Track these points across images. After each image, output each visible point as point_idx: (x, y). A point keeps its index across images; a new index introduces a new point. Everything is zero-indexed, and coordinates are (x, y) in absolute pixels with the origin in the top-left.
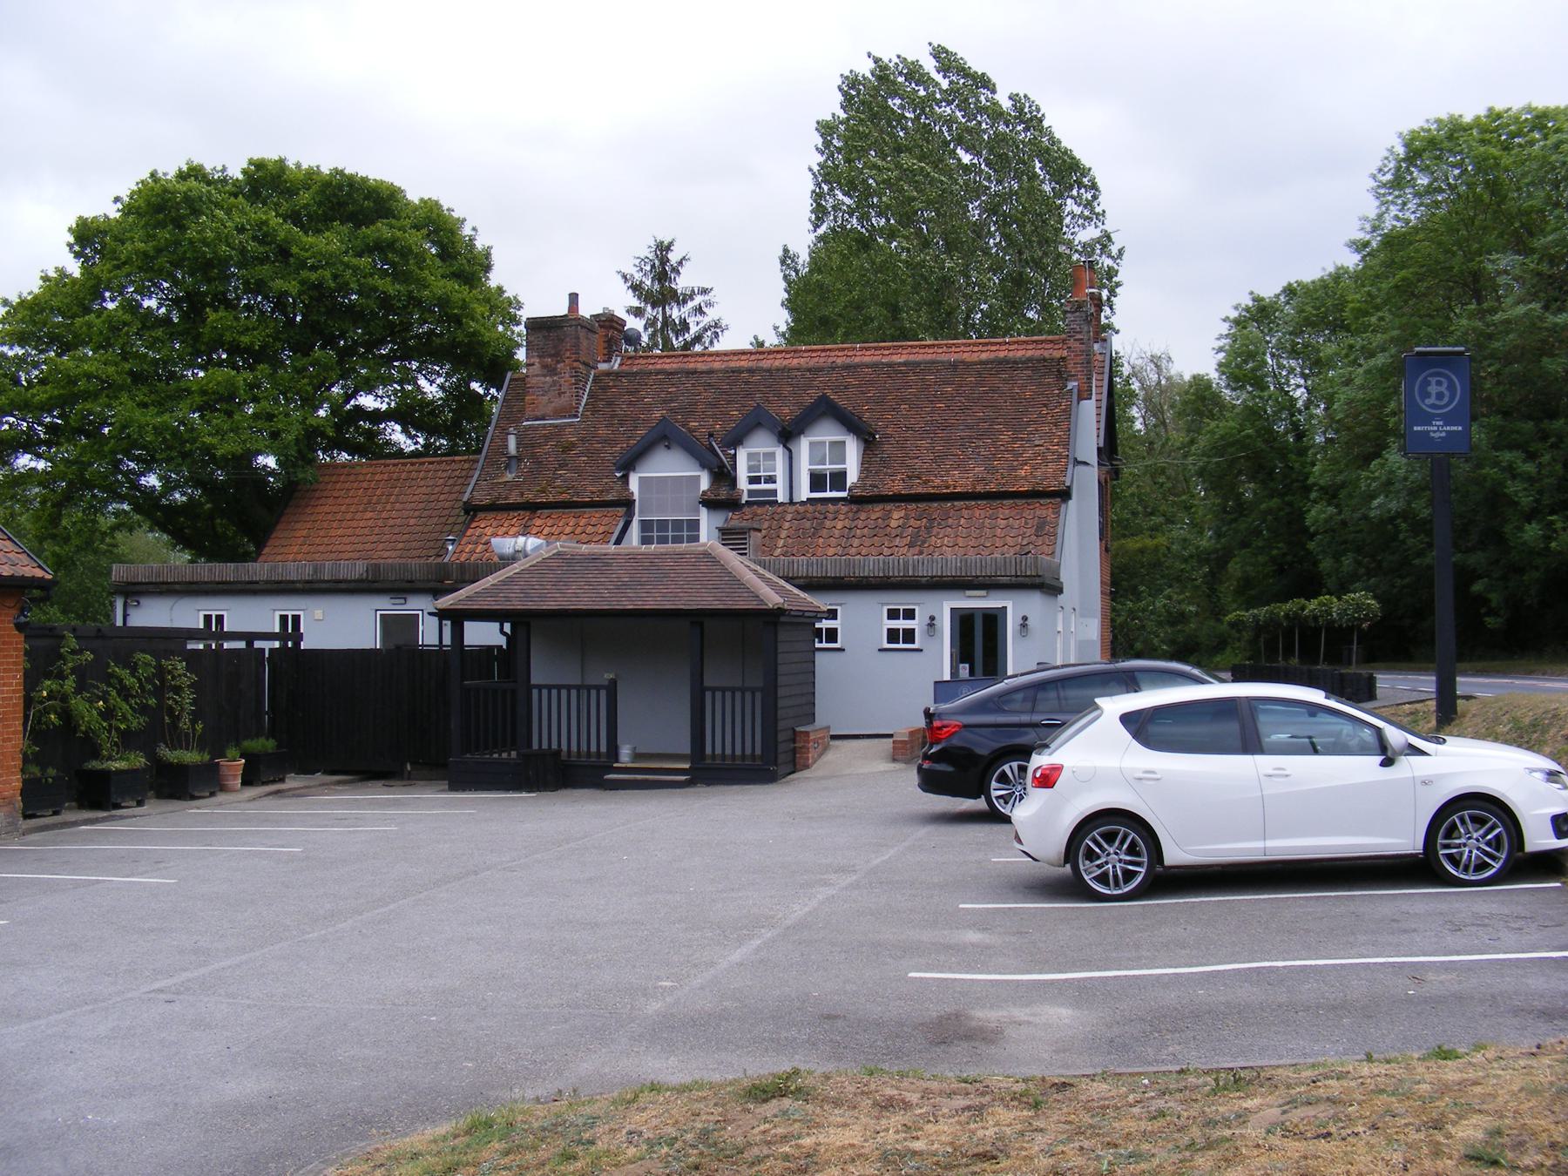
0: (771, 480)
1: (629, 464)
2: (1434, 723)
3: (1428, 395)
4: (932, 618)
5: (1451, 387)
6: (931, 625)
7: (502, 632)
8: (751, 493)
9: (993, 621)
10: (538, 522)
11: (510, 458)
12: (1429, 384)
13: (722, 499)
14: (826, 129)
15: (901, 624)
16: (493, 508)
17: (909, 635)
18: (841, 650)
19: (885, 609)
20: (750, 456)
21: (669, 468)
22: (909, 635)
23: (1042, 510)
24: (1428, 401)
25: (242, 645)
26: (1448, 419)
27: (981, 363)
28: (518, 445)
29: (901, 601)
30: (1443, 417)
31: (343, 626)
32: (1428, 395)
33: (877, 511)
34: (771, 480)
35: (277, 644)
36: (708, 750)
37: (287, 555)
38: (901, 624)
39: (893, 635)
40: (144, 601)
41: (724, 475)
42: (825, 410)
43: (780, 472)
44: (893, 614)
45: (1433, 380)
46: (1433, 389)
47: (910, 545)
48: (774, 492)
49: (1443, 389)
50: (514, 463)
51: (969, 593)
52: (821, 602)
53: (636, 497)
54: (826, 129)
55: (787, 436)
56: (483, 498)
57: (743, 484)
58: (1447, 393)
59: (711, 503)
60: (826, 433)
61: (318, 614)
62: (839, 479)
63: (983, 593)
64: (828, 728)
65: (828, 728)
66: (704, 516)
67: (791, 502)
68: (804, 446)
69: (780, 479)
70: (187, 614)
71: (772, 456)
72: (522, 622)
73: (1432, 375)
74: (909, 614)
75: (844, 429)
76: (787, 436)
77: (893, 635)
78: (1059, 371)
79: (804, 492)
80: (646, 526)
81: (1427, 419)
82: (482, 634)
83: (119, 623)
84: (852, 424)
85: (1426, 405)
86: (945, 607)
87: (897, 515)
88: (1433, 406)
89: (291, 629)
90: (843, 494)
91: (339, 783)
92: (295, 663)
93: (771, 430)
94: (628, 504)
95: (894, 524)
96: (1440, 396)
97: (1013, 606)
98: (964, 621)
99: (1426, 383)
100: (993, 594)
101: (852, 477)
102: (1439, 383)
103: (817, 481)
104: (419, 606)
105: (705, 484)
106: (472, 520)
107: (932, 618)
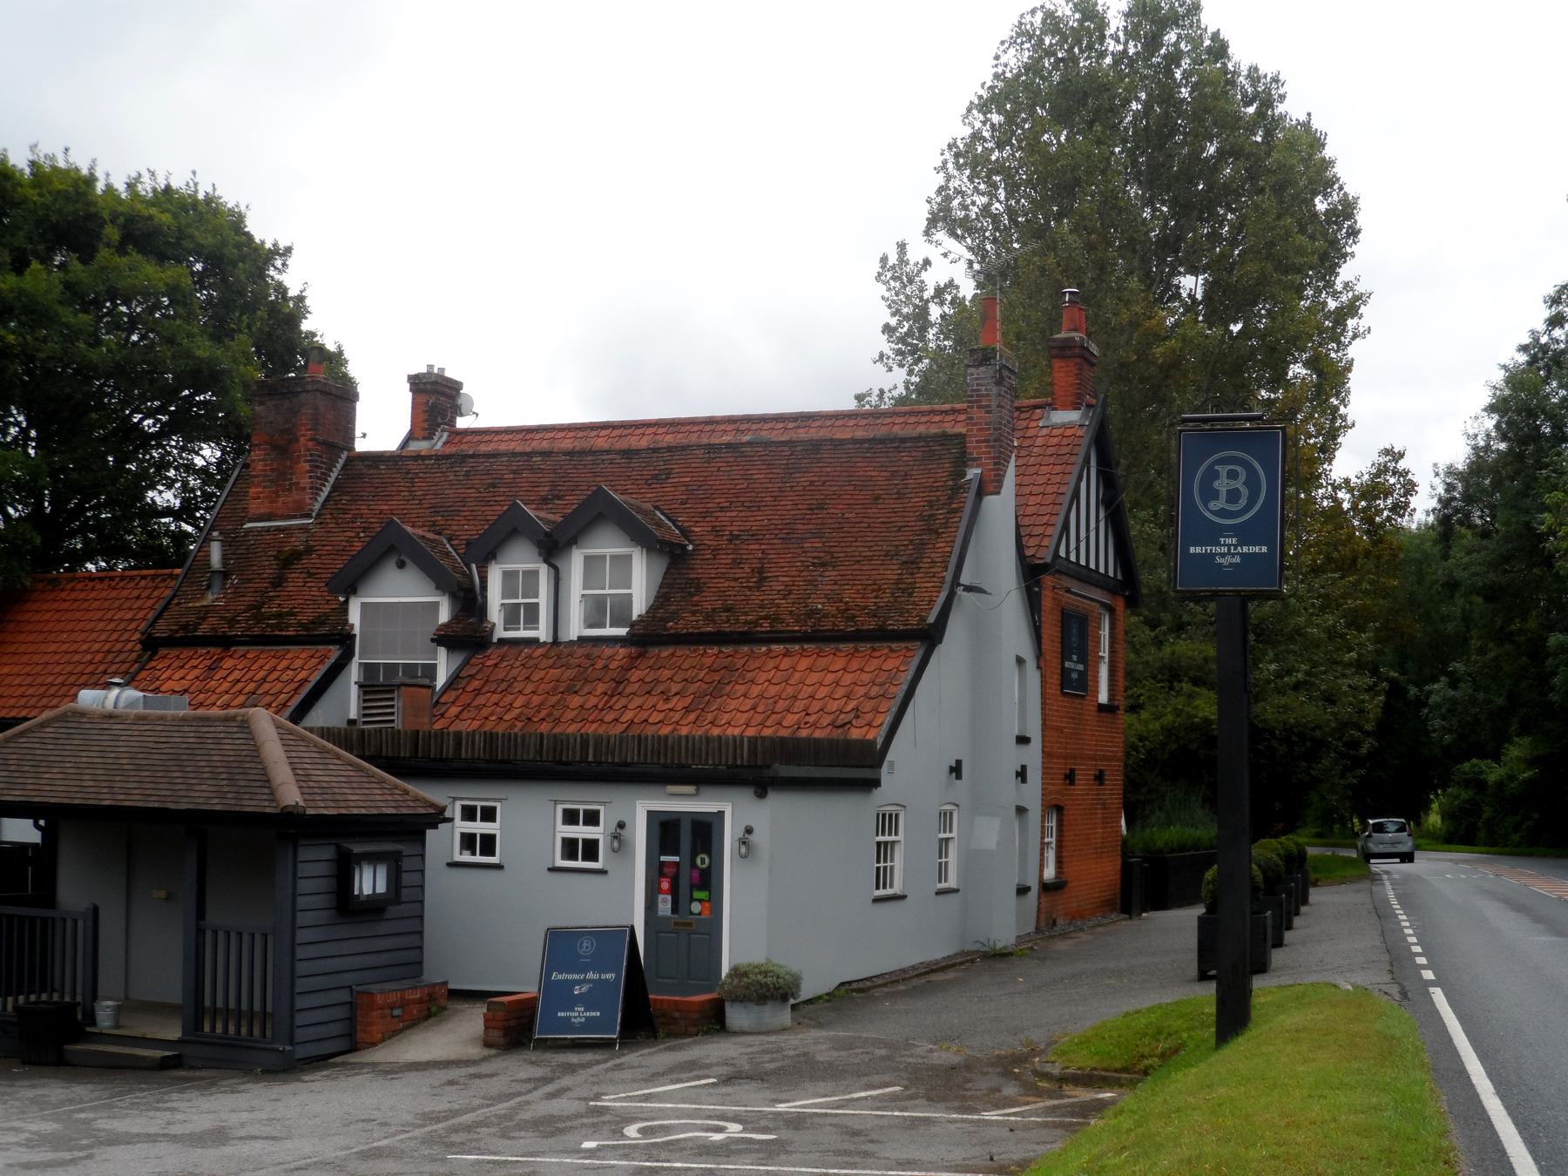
2: (1213, 1041)
3: (1215, 495)
4: (621, 825)
6: (616, 837)
7: (37, 826)
9: (705, 831)
12: (1216, 476)
15: (581, 832)
16: (171, 642)
17: (591, 850)
18: (499, 867)
19: (560, 808)
20: (508, 576)
21: (400, 589)
22: (591, 850)
24: (1214, 505)
26: (1245, 534)
27: (854, 441)
29: (582, 798)
30: (1235, 530)
32: (1215, 495)
36: (207, 1003)
38: (581, 832)
39: (570, 848)
41: (470, 602)
43: (543, 600)
44: (571, 817)
45: (1223, 470)
46: (1222, 485)
47: (687, 710)
49: (1238, 484)
50: (217, 583)
51: (671, 789)
53: (357, 631)
55: (553, 548)
57: (495, 614)
58: (1245, 491)
59: (445, 638)
60: (607, 545)
63: (690, 789)
64: (445, 983)
65: (445, 983)
66: (442, 652)
67: (556, 642)
68: (576, 563)
71: (532, 575)
73: (1223, 461)
74: (592, 818)
77: (570, 848)
80: (368, 669)
81: (1212, 534)
84: (639, 534)
86: (638, 810)
88: (1222, 513)
90: (622, 631)
94: (345, 640)
96: (1233, 496)
97: (732, 810)
98: (665, 830)
99: (1212, 475)
100: (707, 791)
102: (1232, 475)
103: (596, 611)
105: (444, 616)
106: (150, 659)
107: (621, 825)
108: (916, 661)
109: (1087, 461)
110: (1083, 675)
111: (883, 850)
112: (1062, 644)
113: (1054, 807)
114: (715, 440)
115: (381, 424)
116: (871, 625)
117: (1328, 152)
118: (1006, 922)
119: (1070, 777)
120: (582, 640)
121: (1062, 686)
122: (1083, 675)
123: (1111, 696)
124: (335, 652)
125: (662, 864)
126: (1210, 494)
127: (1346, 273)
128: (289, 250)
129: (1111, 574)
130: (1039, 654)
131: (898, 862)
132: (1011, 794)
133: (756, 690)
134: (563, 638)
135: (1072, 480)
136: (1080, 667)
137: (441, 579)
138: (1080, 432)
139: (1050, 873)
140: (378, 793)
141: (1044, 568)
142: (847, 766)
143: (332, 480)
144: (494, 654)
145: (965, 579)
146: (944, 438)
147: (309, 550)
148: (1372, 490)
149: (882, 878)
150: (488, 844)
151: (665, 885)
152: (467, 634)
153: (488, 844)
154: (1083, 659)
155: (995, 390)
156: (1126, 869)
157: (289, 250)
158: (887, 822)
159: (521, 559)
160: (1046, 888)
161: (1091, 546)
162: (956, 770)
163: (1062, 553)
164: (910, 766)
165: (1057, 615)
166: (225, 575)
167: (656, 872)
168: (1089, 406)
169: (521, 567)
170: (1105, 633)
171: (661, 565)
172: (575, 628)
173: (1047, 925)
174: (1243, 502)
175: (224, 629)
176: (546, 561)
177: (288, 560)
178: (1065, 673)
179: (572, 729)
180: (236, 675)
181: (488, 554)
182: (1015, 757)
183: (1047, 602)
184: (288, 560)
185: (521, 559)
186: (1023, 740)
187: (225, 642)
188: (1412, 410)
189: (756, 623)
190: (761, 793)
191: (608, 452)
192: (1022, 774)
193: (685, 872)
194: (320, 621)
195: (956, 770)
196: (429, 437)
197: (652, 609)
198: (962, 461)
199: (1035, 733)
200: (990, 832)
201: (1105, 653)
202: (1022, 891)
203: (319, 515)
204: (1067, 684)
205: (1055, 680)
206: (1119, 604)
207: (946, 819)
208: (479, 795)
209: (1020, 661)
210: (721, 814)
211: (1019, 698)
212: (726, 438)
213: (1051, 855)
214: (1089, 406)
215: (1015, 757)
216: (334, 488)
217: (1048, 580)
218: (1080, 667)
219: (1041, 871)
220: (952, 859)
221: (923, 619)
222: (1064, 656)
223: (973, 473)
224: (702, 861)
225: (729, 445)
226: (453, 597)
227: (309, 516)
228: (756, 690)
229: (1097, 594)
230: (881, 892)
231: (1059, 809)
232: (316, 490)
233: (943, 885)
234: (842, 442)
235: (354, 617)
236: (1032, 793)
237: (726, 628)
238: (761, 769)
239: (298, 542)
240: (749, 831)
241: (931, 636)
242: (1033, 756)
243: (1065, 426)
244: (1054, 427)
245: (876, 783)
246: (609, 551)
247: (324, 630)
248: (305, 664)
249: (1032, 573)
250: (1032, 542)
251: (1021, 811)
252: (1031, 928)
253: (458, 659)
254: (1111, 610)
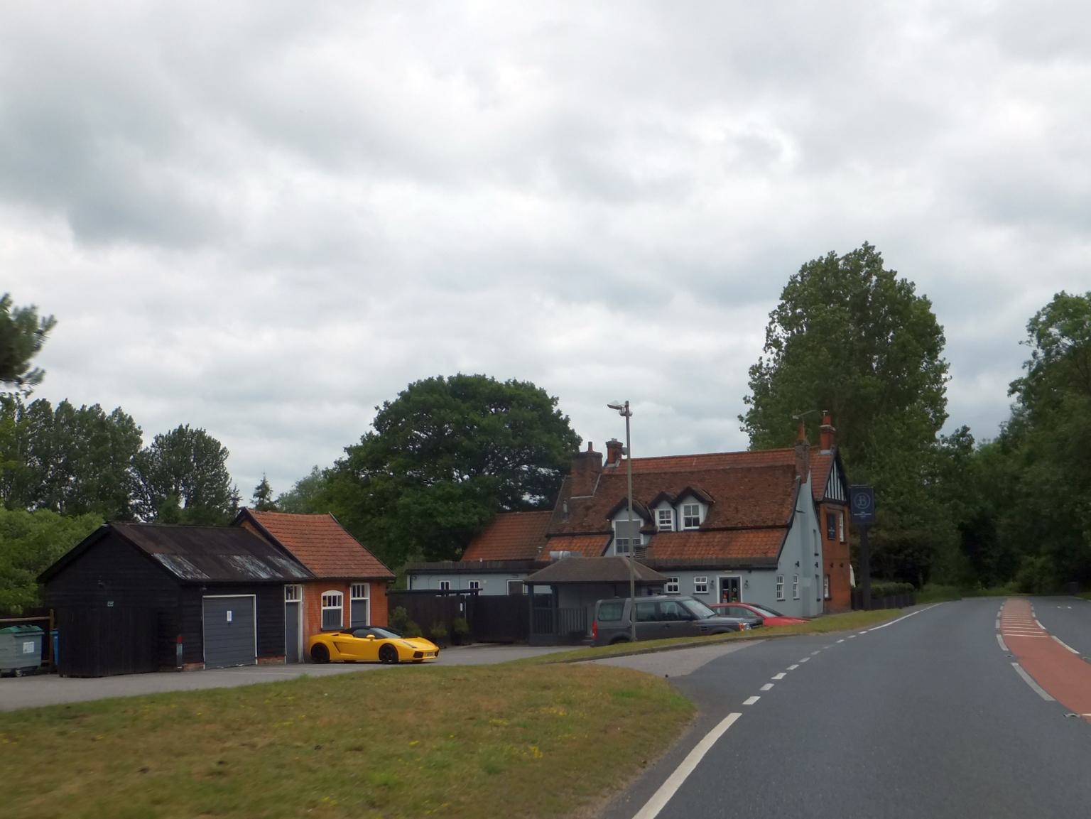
0: (669, 522)
1: (612, 515)
4: (713, 582)
5: (867, 498)
6: (712, 584)
8: (662, 527)
9: (735, 583)
10: (575, 541)
11: (565, 514)
13: (650, 531)
14: (554, 400)
16: (556, 535)
20: (661, 513)
22: (704, 589)
23: (778, 534)
24: (859, 505)
25: (455, 594)
27: (761, 467)
28: (568, 508)
31: (494, 587)
33: (711, 534)
34: (669, 522)
35: (469, 594)
37: (478, 556)
39: (698, 588)
40: (419, 577)
41: (650, 520)
42: (688, 493)
43: (672, 519)
44: (698, 580)
45: (860, 497)
46: (860, 500)
48: (670, 527)
51: (726, 571)
52: (665, 575)
53: (615, 530)
54: (554, 400)
55: (675, 504)
56: (552, 531)
59: (644, 532)
60: (691, 502)
61: (485, 581)
62: (696, 522)
63: (730, 571)
66: (642, 536)
69: (672, 521)
70: (434, 583)
71: (669, 512)
72: (554, 585)
74: (704, 580)
75: (697, 500)
76: (675, 504)
78: (791, 470)
79: (682, 527)
80: (619, 542)
82: (541, 590)
83: (408, 589)
84: (701, 499)
85: (858, 506)
86: (717, 577)
87: (719, 536)
88: (861, 506)
89: (475, 589)
90: (697, 528)
91: (485, 646)
92: (477, 603)
93: (669, 502)
94: (611, 533)
95: (716, 540)
97: (742, 577)
98: (725, 583)
101: (701, 521)
103: (688, 523)
104: (521, 578)
105: (642, 525)
106: (548, 541)
107: (713, 582)
108: (785, 534)
109: (833, 466)
110: (834, 533)
111: (779, 587)
112: (828, 524)
113: (827, 575)
114: (718, 468)
115: (583, 448)
116: (770, 523)
117: (932, 311)
118: (815, 608)
119: (832, 566)
120: (685, 531)
121: (828, 537)
122: (834, 533)
123: (845, 539)
124: (609, 537)
125: (724, 591)
126: (858, 502)
127: (940, 356)
128: (558, 398)
129: (843, 499)
130: (820, 527)
131: (783, 591)
132: (813, 571)
133: (739, 544)
134: (679, 530)
135: (828, 473)
136: (833, 531)
137: (640, 514)
138: (830, 457)
139: (827, 595)
140: (655, 576)
141: (821, 502)
142: (770, 566)
143: (597, 483)
144: (658, 535)
145: (797, 509)
146: (788, 466)
147: (595, 505)
148: (955, 439)
149: (779, 595)
150: (676, 588)
151: (725, 596)
152: (650, 531)
153: (676, 588)
154: (834, 528)
155: (803, 453)
156: (852, 595)
157: (558, 398)
158: (780, 579)
159: (665, 507)
160: (826, 600)
161: (835, 491)
162: (798, 564)
163: (826, 496)
164: (786, 563)
165: (825, 516)
166: (568, 514)
167: (722, 593)
168: (833, 448)
169: (665, 510)
170: (841, 519)
171: (706, 508)
172: (682, 527)
173: (827, 611)
174: (865, 504)
175: (572, 531)
176: (674, 508)
177: (588, 508)
178: (828, 533)
179: (686, 557)
180: (578, 545)
181: (655, 505)
182: (814, 560)
183: (822, 511)
184: (588, 508)
185: (665, 507)
186: (816, 555)
187: (573, 535)
188: (979, 395)
189: (737, 524)
190: (750, 572)
191: (685, 472)
192: (817, 565)
193: (730, 592)
194: (603, 527)
195: (798, 564)
196: (614, 462)
197: (705, 521)
198: (794, 474)
199: (820, 552)
200: (808, 582)
201: (842, 525)
202: (818, 600)
203: (595, 494)
204: (830, 536)
205: (826, 536)
206: (846, 509)
207: (795, 579)
208: (672, 575)
209: (815, 531)
210: (739, 578)
211: (815, 542)
212: (722, 468)
213: (827, 590)
214: (833, 448)
215: (814, 560)
216: (598, 486)
217: (822, 505)
218: (833, 531)
219: (824, 594)
220: (797, 590)
221: (786, 522)
222: (828, 528)
223: (798, 477)
224: (735, 590)
225: (722, 469)
226: (645, 519)
227: (592, 495)
228: (739, 544)
229: (838, 507)
230: (779, 599)
231: (829, 576)
232: (594, 487)
233: (795, 598)
234: (757, 468)
235: (614, 526)
236: (820, 571)
237: (729, 526)
238: (748, 567)
239: (589, 504)
240: (747, 581)
241: (788, 527)
242: (820, 559)
243: (826, 455)
244: (822, 455)
245: (776, 568)
246: (692, 504)
247: (605, 530)
248: (600, 541)
249: (817, 504)
250: (817, 494)
251: (817, 576)
252: (822, 611)
253: (648, 537)
254: (844, 512)
